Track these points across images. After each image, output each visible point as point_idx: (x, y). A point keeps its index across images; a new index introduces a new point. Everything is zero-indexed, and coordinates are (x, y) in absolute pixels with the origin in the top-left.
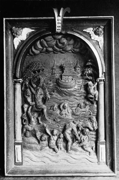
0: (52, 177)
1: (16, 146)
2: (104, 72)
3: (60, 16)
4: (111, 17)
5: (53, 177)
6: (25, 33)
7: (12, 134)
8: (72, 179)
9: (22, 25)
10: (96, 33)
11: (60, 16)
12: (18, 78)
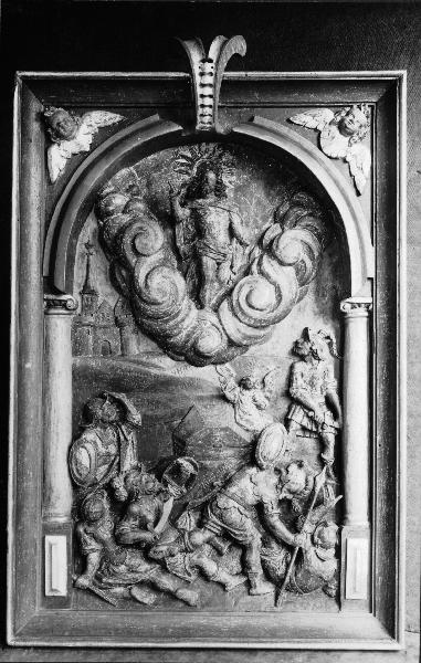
0: (174, 652)
1: (49, 538)
3: (211, 61)
5: (179, 652)
8: (247, 660)
9: (81, 99)
10: (342, 127)
11: (211, 61)
12: (60, 293)
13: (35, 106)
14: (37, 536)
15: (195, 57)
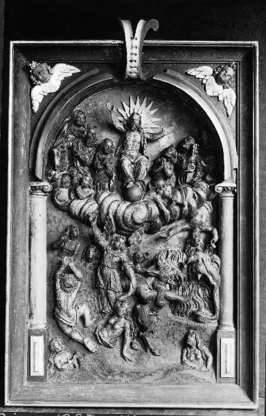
1: (33, 339)
2: (236, 169)
4: (253, 42)
6: (61, 72)
9: (52, 57)
10: (218, 79)
13: (23, 60)
15: (127, 27)
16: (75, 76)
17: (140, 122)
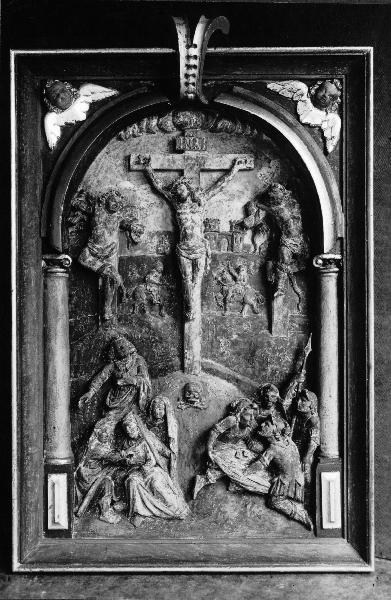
1: (53, 478)
2: (341, 239)
3: (195, 46)
6: (92, 93)
7: (36, 435)
9: (79, 73)
10: (318, 102)
11: (195, 46)
14: (39, 476)
16: (112, 98)
17: (202, 305)
